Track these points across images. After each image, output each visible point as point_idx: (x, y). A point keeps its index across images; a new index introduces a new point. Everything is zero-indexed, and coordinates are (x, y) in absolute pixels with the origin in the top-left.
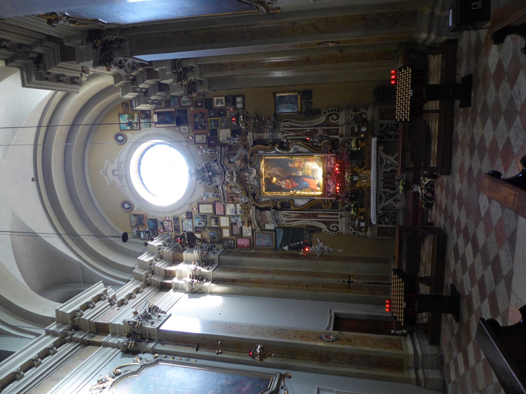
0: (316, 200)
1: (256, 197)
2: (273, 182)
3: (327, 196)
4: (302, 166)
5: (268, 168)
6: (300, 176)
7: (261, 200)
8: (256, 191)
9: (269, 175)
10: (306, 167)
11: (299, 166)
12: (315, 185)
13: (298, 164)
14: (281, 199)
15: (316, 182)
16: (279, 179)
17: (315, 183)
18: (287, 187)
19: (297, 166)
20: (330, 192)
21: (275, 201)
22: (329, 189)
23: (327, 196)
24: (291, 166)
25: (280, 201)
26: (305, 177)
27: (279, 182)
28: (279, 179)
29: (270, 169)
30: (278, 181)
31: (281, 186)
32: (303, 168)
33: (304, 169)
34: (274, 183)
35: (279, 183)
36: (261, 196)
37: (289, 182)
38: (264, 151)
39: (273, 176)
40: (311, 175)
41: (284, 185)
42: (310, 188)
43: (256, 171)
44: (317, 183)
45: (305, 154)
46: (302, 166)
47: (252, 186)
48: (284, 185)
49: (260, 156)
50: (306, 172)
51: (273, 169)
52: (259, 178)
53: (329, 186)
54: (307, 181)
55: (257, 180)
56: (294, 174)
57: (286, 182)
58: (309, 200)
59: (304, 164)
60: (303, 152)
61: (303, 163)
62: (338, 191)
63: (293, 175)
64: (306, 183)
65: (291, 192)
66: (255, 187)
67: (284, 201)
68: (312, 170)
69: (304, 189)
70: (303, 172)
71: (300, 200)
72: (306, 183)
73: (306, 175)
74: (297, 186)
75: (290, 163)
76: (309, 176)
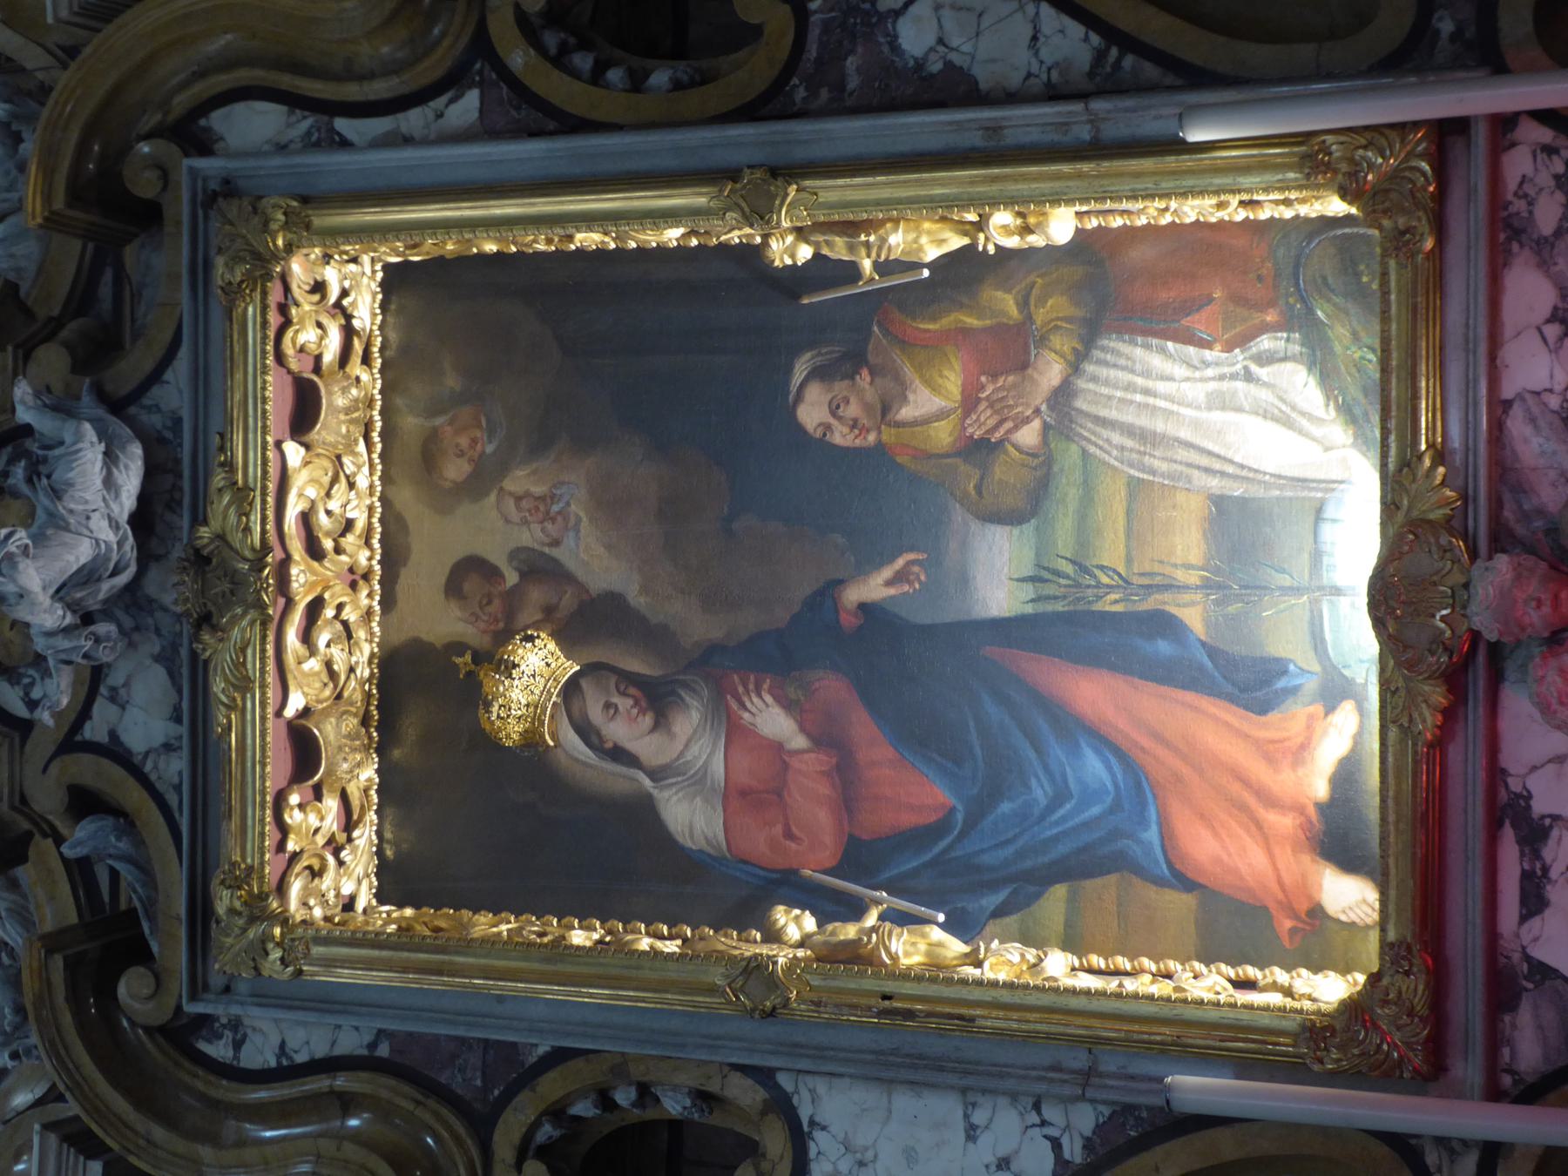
0: (1226, 1146)
1: (131, 988)
2: (512, 732)
3: (1468, 1069)
4: (1028, 435)
5: (455, 470)
6: (1004, 629)
7: (219, 1050)
8: (144, 869)
9: (454, 587)
10: (1110, 447)
11: (982, 423)
12: (1284, 823)
13: (953, 382)
14: (559, 1056)
15: (1301, 752)
16: (628, 680)
17: (1282, 781)
18: (760, 842)
19: (943, 435)
20: (1542, 972)
21: (466, 1080)
22: (1534, 901)
23: (1468, 1069)
24: (841, 437)
25: (551, 1086)
26: (1095, 659)
27: (618, 731)
28: (628, 680)
29: (481, 481)
30: (596, 714)
31: (643, 813)
32: (1043, 467)
33: (1068, 490)
34: (532, 739)
35: (618, 754)
36: (218, 968)
37: (799, 742)
38: (293, 101)
39: (529, 614)
40: (1194, 616)
41: (698, 782)
42: (1184, 882)
43: (131, 481)
44: (1321, 789)
45: (1029, 120)
46: (1028, 435)
47: (88, 770)
48: (698, 782)
49: (229, 188)
50: (1111, 552)
51: (520, 480)
52: (205, 620)
53: (1534, 834)
54: (1118, 723)
55: (167, 659)
56: (874, 588)
57: (736, 733)
58: (1085, 1119)
59: (1063, 395)
60: (984, 76)
61: (1051, 372)
62: (477, 78)
63: (863, 607)
64: (1094, 767)
65: (796, 923)
66: (133, 796)
67: (624, 1096)
68: (1220, 503)
69: (1057, 896)
70: (1043, 547)
71: (904, 1101)
72: (1094, 767)
73: (1111, 603)
74: (937, 830)
75: (820, 373)
76: (1165, 624)
